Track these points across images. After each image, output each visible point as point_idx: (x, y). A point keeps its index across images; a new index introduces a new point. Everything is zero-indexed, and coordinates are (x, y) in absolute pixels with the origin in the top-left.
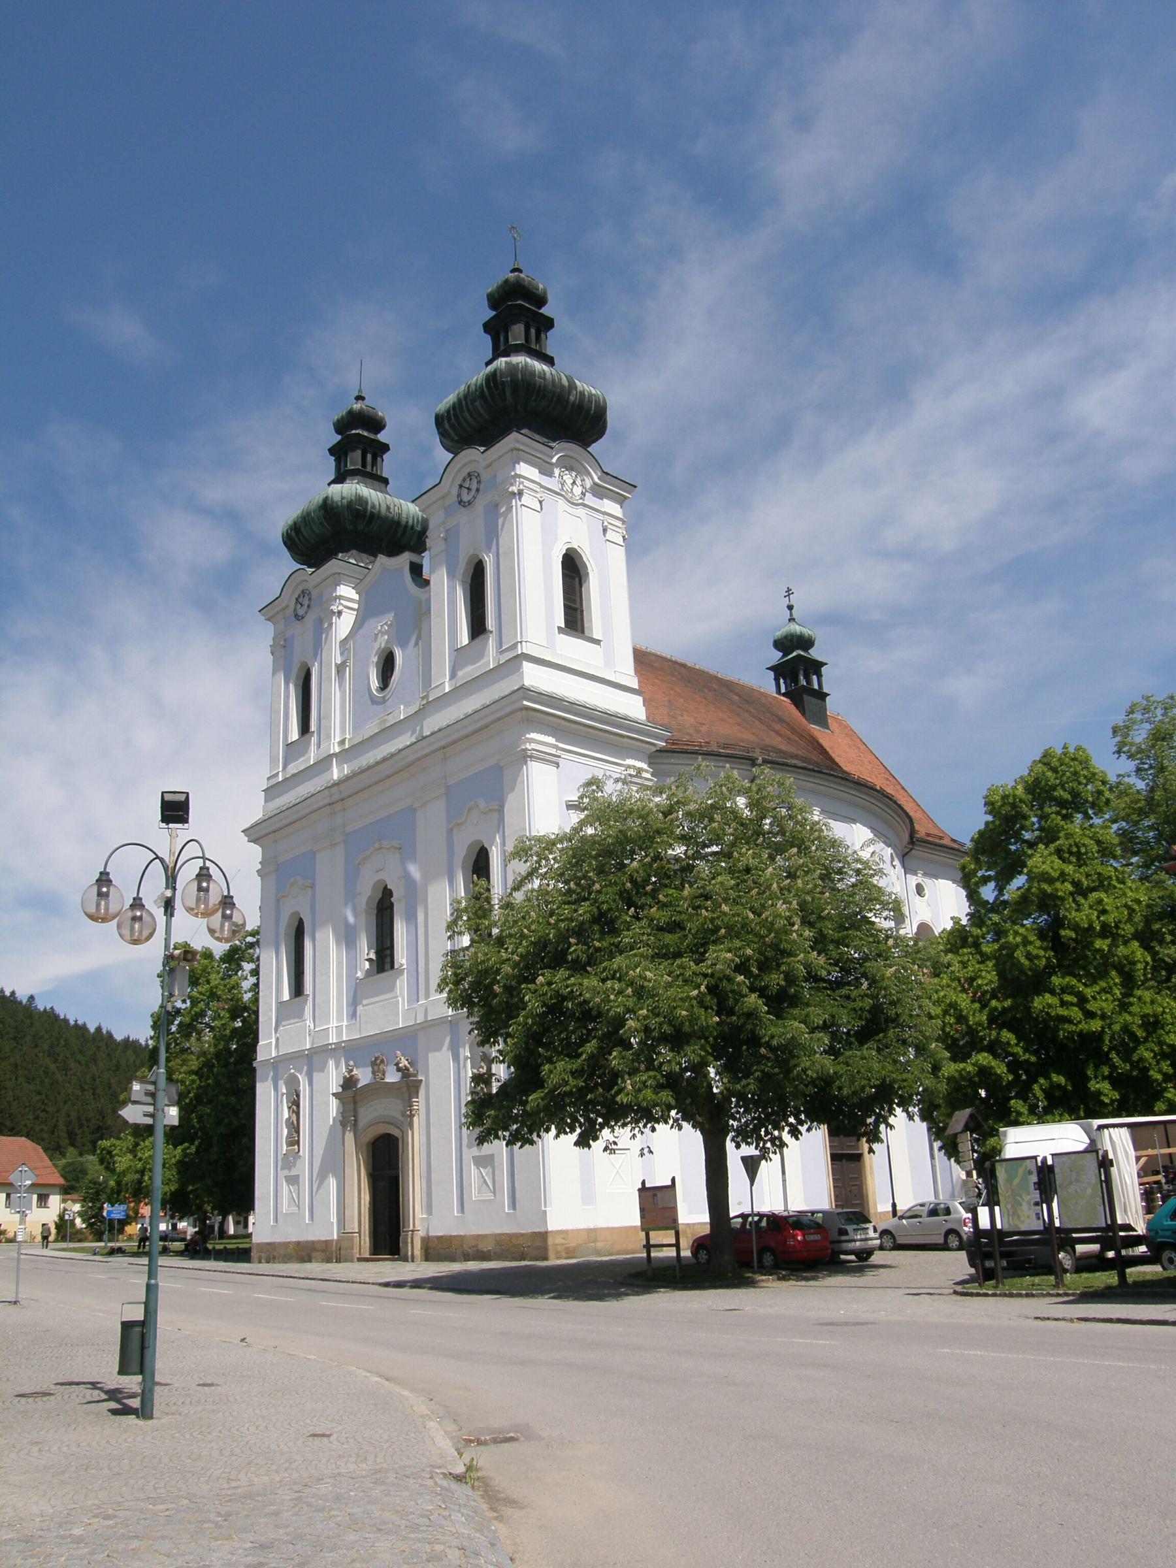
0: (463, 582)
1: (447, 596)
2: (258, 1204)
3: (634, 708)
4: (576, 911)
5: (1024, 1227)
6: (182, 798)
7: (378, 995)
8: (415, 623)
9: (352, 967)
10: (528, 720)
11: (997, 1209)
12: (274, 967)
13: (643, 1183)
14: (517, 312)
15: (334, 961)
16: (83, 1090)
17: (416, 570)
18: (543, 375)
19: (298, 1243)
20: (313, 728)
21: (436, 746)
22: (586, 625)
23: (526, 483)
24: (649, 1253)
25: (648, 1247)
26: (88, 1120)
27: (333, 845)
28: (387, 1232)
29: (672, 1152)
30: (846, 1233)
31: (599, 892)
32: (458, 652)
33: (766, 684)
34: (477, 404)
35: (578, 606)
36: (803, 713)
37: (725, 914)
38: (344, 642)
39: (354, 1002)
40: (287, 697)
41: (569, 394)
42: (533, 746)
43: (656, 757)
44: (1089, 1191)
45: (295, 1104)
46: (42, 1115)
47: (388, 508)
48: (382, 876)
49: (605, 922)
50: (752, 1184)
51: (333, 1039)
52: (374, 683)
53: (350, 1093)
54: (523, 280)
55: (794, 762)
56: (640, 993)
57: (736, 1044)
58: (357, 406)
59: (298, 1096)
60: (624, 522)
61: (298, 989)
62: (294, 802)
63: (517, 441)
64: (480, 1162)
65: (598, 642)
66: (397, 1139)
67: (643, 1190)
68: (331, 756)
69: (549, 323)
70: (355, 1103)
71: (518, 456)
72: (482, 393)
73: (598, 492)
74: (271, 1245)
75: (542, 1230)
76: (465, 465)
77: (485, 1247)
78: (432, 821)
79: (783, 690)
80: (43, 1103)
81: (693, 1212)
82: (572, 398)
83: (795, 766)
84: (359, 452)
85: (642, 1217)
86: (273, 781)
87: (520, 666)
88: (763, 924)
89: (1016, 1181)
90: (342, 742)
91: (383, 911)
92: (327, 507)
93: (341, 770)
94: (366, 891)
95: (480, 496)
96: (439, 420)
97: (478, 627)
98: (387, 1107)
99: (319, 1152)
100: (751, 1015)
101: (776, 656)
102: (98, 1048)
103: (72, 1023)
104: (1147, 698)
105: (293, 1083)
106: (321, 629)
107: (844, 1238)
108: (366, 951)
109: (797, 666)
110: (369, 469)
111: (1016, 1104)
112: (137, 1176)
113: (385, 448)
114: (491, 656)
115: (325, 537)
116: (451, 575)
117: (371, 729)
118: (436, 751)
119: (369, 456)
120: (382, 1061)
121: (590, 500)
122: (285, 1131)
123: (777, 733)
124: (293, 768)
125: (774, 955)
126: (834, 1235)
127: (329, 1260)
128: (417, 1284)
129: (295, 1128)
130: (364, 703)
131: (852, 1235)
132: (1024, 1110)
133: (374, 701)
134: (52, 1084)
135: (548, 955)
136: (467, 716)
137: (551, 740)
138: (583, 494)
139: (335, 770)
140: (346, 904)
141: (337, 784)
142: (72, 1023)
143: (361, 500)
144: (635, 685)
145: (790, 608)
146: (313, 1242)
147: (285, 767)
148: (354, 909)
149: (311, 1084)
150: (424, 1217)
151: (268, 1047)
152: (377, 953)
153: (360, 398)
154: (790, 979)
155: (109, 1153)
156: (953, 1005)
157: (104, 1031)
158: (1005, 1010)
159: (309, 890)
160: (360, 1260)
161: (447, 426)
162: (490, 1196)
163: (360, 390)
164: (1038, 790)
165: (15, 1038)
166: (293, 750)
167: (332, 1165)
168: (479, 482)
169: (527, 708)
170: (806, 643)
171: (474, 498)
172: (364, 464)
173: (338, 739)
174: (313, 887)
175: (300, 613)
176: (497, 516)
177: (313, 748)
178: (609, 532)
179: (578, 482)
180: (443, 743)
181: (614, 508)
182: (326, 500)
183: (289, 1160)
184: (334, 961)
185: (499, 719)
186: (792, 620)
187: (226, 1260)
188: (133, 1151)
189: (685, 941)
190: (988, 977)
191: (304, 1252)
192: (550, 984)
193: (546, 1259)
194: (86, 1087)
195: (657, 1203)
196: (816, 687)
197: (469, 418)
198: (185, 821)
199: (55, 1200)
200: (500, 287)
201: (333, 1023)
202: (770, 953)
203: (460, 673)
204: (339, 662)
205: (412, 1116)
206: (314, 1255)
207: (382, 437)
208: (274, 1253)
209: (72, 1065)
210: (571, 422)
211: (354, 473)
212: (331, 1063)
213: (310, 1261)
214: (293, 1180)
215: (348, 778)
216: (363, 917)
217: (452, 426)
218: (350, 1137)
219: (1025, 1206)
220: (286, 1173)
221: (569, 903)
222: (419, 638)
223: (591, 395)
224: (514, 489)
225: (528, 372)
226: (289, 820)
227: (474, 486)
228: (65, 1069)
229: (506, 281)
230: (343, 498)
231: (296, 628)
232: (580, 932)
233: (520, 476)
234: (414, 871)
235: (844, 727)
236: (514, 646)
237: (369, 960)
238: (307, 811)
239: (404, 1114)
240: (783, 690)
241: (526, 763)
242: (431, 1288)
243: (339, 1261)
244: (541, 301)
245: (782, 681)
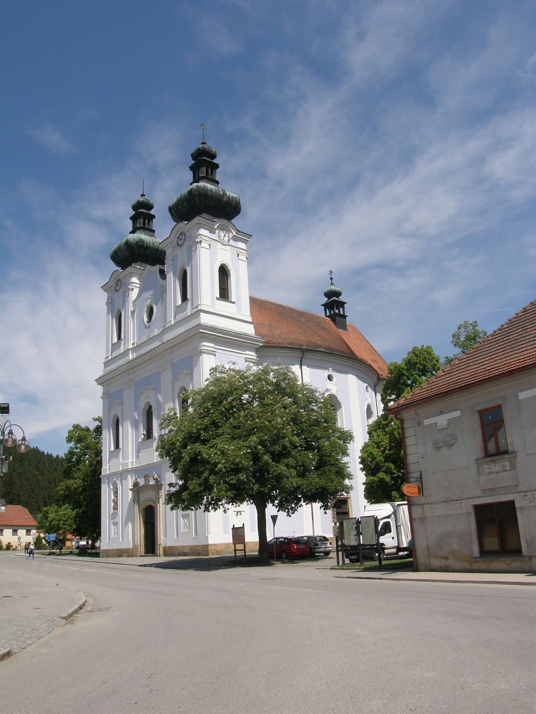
0: (179, 278)
1: (173, 283)
2: (102, 534)
3: (250, 330)
4: (203, 421)
5: (351, 544)
6: (6, 406)
7: (146, 449)
8: (161, 295)
9: (137, 437)
10: (202, 337)
11: (361, 536)
12: (107, 438)
13: (234, 526)
14: (204, 163)
15: (130, 435)
16: (50, 483)
17: (162, 273)
18: (211, 190)
19: (117, 550)
20: (122, 338)
21: (167, 347)
22: (229, 296)
23: (203, 237)
24: (235, 553)
25: (235, 550)
26: (53, 497)
27: (130, 387)
28: (151, 545)
29: (245, 514)
30: (317, 545)
31: (213, 413)
32: (177, 307)
33: (320, 312)
34: (185, 203)
35: (226, 288)
36: (336, 324)
37: (257, 423)
38: (134, 302)
39: (138, 452)
40: (112, 324)
41: (223, 198)
42: (205, 348)
43: (258, 350)
44: (371, 531)
45: (116, 493)
46: (33, 495)
47: (153, 243)
48: (148, 400)
49: (215, 425)
50: (274, 526)
51: (130, 466)
52: (146, 319)
53: (136, 489)
54: (206, 148)
55: (322, 350)
56: (223, 453)
57: (261, 474)
58: (141, 199)
59: (117, 490)
60: (246, 251)
61: (117, 446)
62: (115, 368)
63: (199, 220)
64: (184, 517)
65: (234, 303)
66: (154, 507)
67: (234, 528)
68: (129, 349)
69: (217, 166)
70: (138, 493)
71: (200, 226)
72: (186, 198)
73: (235, 239)
74: (107, 551)
75: (206, 544)
76: (179, 229)
77: (186, 550)
78: (167, 377)
79: (328, 314)
80: (33, 490)
81: (252, 536)
82: (224, 199)
83: (320, 351)
84: (142, 219)
85: (233, 539)
86: (107, 359)
87: (200, 315)
88: (272, 426)
89: (349, 527)
90: (133, 344)
91: (149, 414)
92: (128, 244)
93: (133, 355)
94: (142, 406)
95: (185, 242)
96: (171, 209)
97: (184, 298)
98: (150, 494)
99: (125, 513)
100: (267, 463)
101: (325, 300)
102: (58, 465)
103: (46, 454)
104: (465, 322)
105: (115, 484)
106: (125, 296)
107: (316, 547)
108: (142, 431)
109: (334, 303)
110: (146, 226)
111: (394, 493)
112: (57, 522)
113: (154, 217)
114: (189, 311)
115: (129, 256)
116: (174, 275)
117: (144, 338)
118: (167, 349)
119: (146, 221)
120: (148, 476)
121: (232, 242)
122: (112, 504)
123: (319, 336)
124: (115, 354)
125: (277, 438)
126: (312, 546)
127: (129, 556)
128: (151, 565)
129: (116, 503)
130: (143, 328)
131: (320, 546)
132: (398, 496)
133: (146, 327)
134: (36, 481)
135: (193, 438)
136: (179, 335)
137: (212, 345)
138: (229, 240)
139: (131, 355)
140: (135, 411)
141: (132, 361)
142: (46, 454)
143: (141, 241)
145: (331, 279)
146: (123, 549)
147: (112, 353)
148: (138, 413)
149: (122, 485)
150: (165, 538)
151: (106, 469)
152: (147, 432)
153: (143, 195)
154: (284, 447)
155: (47, 512)
156: (371, 453)
157: (60, 457)
158: (391, 455)
159: (121, 406)
160: (141, 556)
161: (173, 212)
162: (188, 530)
163: (143, 192)
164: (410, 364)
165: (20, 461)
166: (115, 347)
167: (130, 518)
168: (185, 236)
169: (202, 332)
170: (338, 294)
171: (183, 243)
172: (144, 225)
173: (132, 342)
174: (122, 404)
175: (116, 289)
176: (192, 251)
177: (122, 346)
178: (240, 256)
179: (227, 235)
180: (170, 346)
181: (242, 245)
182: (127, 241)
183: (114, 516)
184: (130, 435)
185: (191, 337)
186: (332, 284)
187: (92, 557)
188: (57, 512)
189: (240, 434)
190: (386, 441)
191: (120, 553)
192: (192, 449)
193: (208, 555)
194: (51, 482)
195: (238, 534)
196: (342, 313)
197: (182, 209)
198: (8, 413)
199: (34, 532)
200: (196, 151)
201: (130, 460)
202: (275, 438)
203: (177, 317)
204: (132, 310)
205: (159, 498)
206: (123, 554)
207: (152, 212)
208: (109, 554)
209: (46, 472)
210: (224, 210)
211: (140, 228)
212: (129, 476)
213: (122, 556)
214: (115, 524)
215: (134, 359)
216: (141, 417)
217: (175, 212)
218: (136, 506)
219: (352, 536)
220: (113, 521)
221: (200, 418)
222: (162, 301)
223: (233, 197)
224: (198, 240)
225: (205, 189)
226: (113, 376)
227: (183, 238)
228: (43, 474)
229: (198, 149)
230: (134, 240)
231: (116, 295)
232: (206, 429)
233: (201, 235)
234: (160, 397)
235: (355, 329)
236: (197, 306)
237: (143, 434)
238: (119, 373)
239: (156, 498)
240: (328, 314)
241: (201, 355)
242: (155, 567)
243: (132, 557)
244: (214, 156)
245: (327, 310)
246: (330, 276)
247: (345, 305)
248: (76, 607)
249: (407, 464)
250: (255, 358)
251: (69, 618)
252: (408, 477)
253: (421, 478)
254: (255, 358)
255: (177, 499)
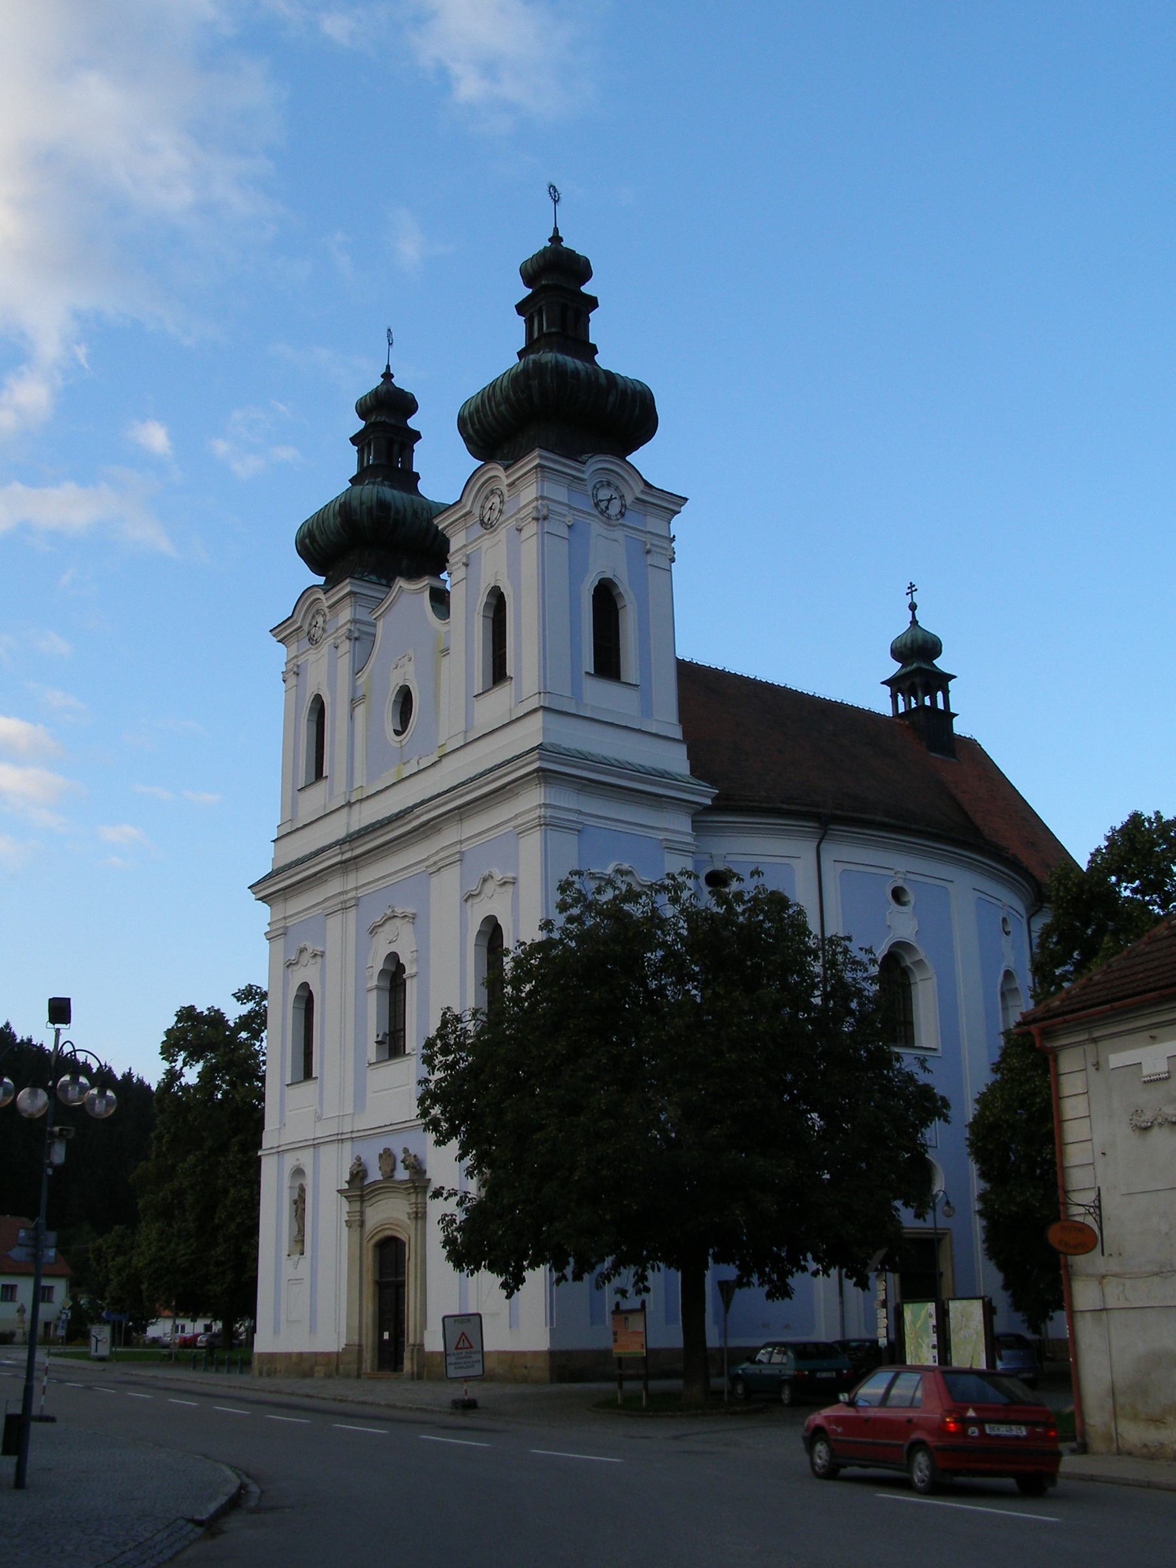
19: (301, 1354)
47: (415, 513)
66: (404, 1244)
144: (679, 736)
145: (913, 607)
196: (941, 706)
225: (559, 371)
230: (362, 503)
245: (900, 697)
246: (908, 599)
247: (951, 684)
248: (222, 1499)
249: (1064, 1168)
250: (689, 840)
251: (211, 1526)
252: (1065, 1204)
253: (1099, 1207)
254: (689, 840)
255: (466, 1253)
